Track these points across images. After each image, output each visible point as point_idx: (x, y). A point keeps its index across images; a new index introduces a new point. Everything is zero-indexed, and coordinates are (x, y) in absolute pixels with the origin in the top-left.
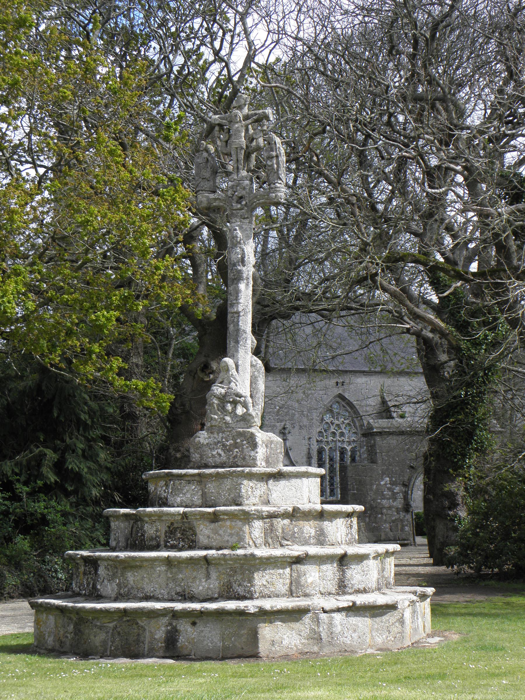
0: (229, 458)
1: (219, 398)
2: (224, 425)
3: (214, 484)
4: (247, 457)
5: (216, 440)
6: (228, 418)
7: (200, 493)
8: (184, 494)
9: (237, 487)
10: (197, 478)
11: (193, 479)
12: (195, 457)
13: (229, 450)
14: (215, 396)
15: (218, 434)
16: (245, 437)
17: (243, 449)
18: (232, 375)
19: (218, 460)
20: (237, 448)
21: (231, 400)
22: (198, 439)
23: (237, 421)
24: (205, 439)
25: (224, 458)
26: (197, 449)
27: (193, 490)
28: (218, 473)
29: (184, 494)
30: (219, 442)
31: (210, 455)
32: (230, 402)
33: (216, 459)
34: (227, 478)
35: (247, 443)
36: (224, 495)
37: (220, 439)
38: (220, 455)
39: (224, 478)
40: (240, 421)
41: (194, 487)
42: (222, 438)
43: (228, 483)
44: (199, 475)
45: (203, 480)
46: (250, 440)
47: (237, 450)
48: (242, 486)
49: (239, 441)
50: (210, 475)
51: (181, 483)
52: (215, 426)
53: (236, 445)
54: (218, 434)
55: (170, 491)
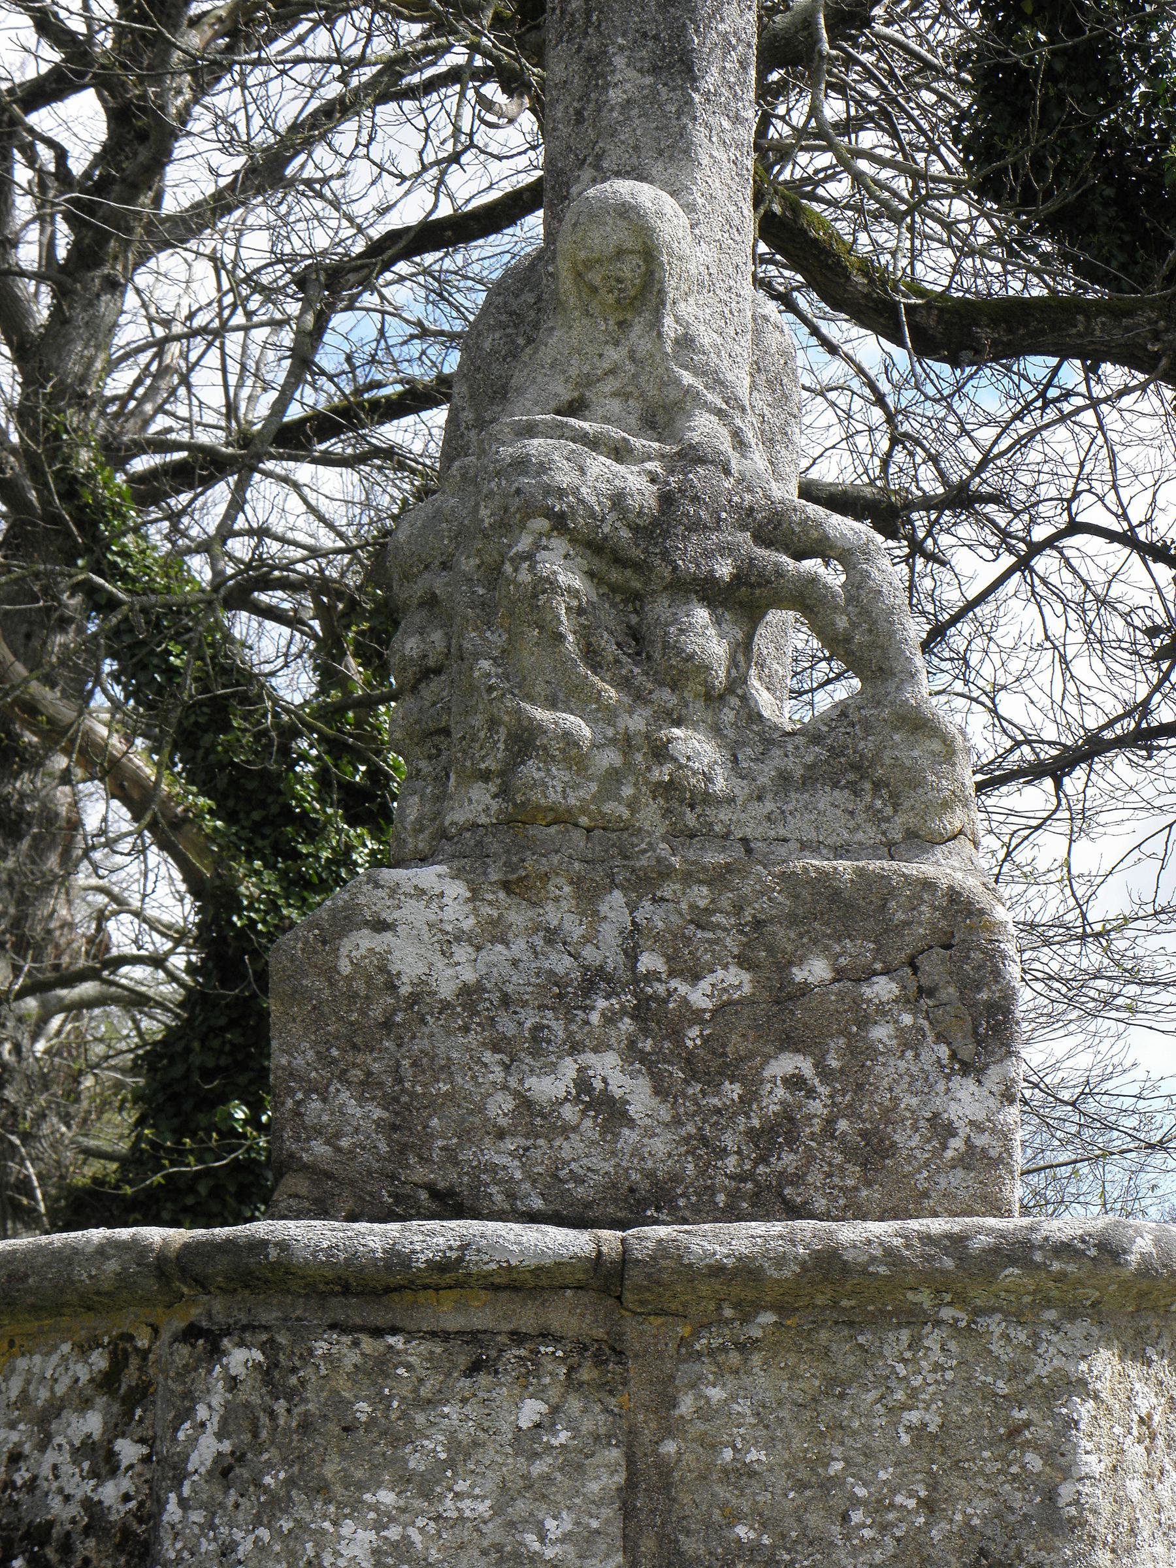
0: (705, 1146)
1: (595, 548)
2: (650, 815)
3: (764, 1381)
4: (907, 1139)
5: (562, 964)
6: (696, 747)
7: (605, 1476)
8: (425, 1486)
9: (1029, 1425)
10: (568, 1316)
11: (527, 1318)
12: (344, 1119)
13: (708, 1068)
14: (560, 522)
15: (588, 897)
16: (885, 933)
17: (861, 1053)
18: (686, 342)
19: (583, 1154)
20: (790, 1042)
21: (724, 569)
22: (363, 942)
23: (784, 779)
24: (448, 941)
25: (653, 1135)
26: (356, 1040)
27: (527, 1442)
28: (829, 1264)
29: (425, 1486)
30: (595, 979)
31: (500, 1106)
32: (709, 591)
33: (568, 1148)
34: (914, 1318)
35: (907, 1001)
36: (878, 1506)
37: (606, 952)
38: (610, 1111)
39: (879, 1320)
40: (810, 779)
41: (531, 1411)
42: (634, 940)
43: (922, 1379)
44: (606, 1278)
45: (638, 1333)
46: (934, 966)
47: (787, 1064)
48: (1085, 1410)
49: (815, 970)
50: (742, 1279)
51: (381, 1367)
52: (563, 818)
53: (783, 1014)
54: (588, 897)
55: (206, 1450)
